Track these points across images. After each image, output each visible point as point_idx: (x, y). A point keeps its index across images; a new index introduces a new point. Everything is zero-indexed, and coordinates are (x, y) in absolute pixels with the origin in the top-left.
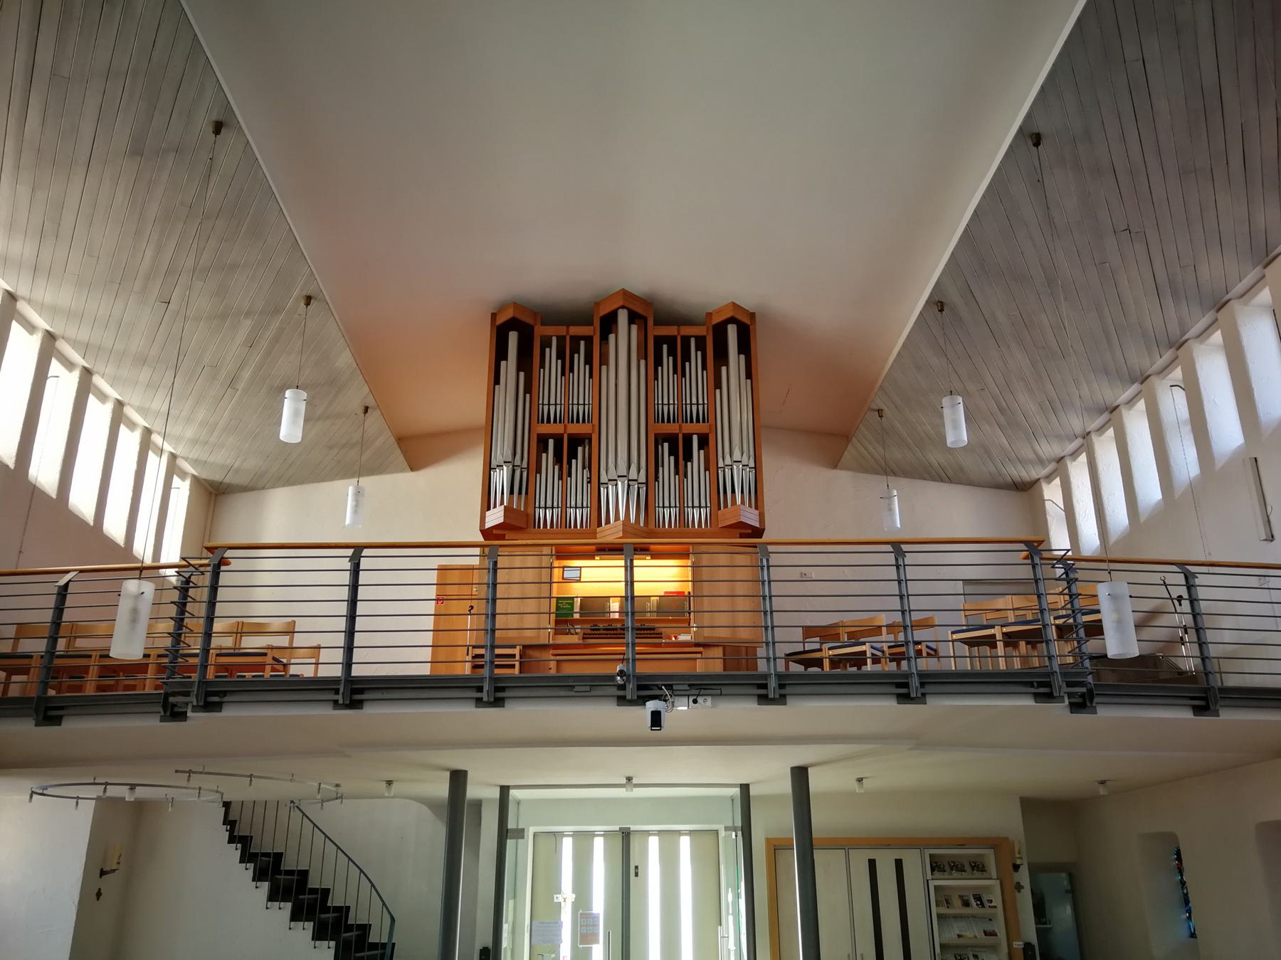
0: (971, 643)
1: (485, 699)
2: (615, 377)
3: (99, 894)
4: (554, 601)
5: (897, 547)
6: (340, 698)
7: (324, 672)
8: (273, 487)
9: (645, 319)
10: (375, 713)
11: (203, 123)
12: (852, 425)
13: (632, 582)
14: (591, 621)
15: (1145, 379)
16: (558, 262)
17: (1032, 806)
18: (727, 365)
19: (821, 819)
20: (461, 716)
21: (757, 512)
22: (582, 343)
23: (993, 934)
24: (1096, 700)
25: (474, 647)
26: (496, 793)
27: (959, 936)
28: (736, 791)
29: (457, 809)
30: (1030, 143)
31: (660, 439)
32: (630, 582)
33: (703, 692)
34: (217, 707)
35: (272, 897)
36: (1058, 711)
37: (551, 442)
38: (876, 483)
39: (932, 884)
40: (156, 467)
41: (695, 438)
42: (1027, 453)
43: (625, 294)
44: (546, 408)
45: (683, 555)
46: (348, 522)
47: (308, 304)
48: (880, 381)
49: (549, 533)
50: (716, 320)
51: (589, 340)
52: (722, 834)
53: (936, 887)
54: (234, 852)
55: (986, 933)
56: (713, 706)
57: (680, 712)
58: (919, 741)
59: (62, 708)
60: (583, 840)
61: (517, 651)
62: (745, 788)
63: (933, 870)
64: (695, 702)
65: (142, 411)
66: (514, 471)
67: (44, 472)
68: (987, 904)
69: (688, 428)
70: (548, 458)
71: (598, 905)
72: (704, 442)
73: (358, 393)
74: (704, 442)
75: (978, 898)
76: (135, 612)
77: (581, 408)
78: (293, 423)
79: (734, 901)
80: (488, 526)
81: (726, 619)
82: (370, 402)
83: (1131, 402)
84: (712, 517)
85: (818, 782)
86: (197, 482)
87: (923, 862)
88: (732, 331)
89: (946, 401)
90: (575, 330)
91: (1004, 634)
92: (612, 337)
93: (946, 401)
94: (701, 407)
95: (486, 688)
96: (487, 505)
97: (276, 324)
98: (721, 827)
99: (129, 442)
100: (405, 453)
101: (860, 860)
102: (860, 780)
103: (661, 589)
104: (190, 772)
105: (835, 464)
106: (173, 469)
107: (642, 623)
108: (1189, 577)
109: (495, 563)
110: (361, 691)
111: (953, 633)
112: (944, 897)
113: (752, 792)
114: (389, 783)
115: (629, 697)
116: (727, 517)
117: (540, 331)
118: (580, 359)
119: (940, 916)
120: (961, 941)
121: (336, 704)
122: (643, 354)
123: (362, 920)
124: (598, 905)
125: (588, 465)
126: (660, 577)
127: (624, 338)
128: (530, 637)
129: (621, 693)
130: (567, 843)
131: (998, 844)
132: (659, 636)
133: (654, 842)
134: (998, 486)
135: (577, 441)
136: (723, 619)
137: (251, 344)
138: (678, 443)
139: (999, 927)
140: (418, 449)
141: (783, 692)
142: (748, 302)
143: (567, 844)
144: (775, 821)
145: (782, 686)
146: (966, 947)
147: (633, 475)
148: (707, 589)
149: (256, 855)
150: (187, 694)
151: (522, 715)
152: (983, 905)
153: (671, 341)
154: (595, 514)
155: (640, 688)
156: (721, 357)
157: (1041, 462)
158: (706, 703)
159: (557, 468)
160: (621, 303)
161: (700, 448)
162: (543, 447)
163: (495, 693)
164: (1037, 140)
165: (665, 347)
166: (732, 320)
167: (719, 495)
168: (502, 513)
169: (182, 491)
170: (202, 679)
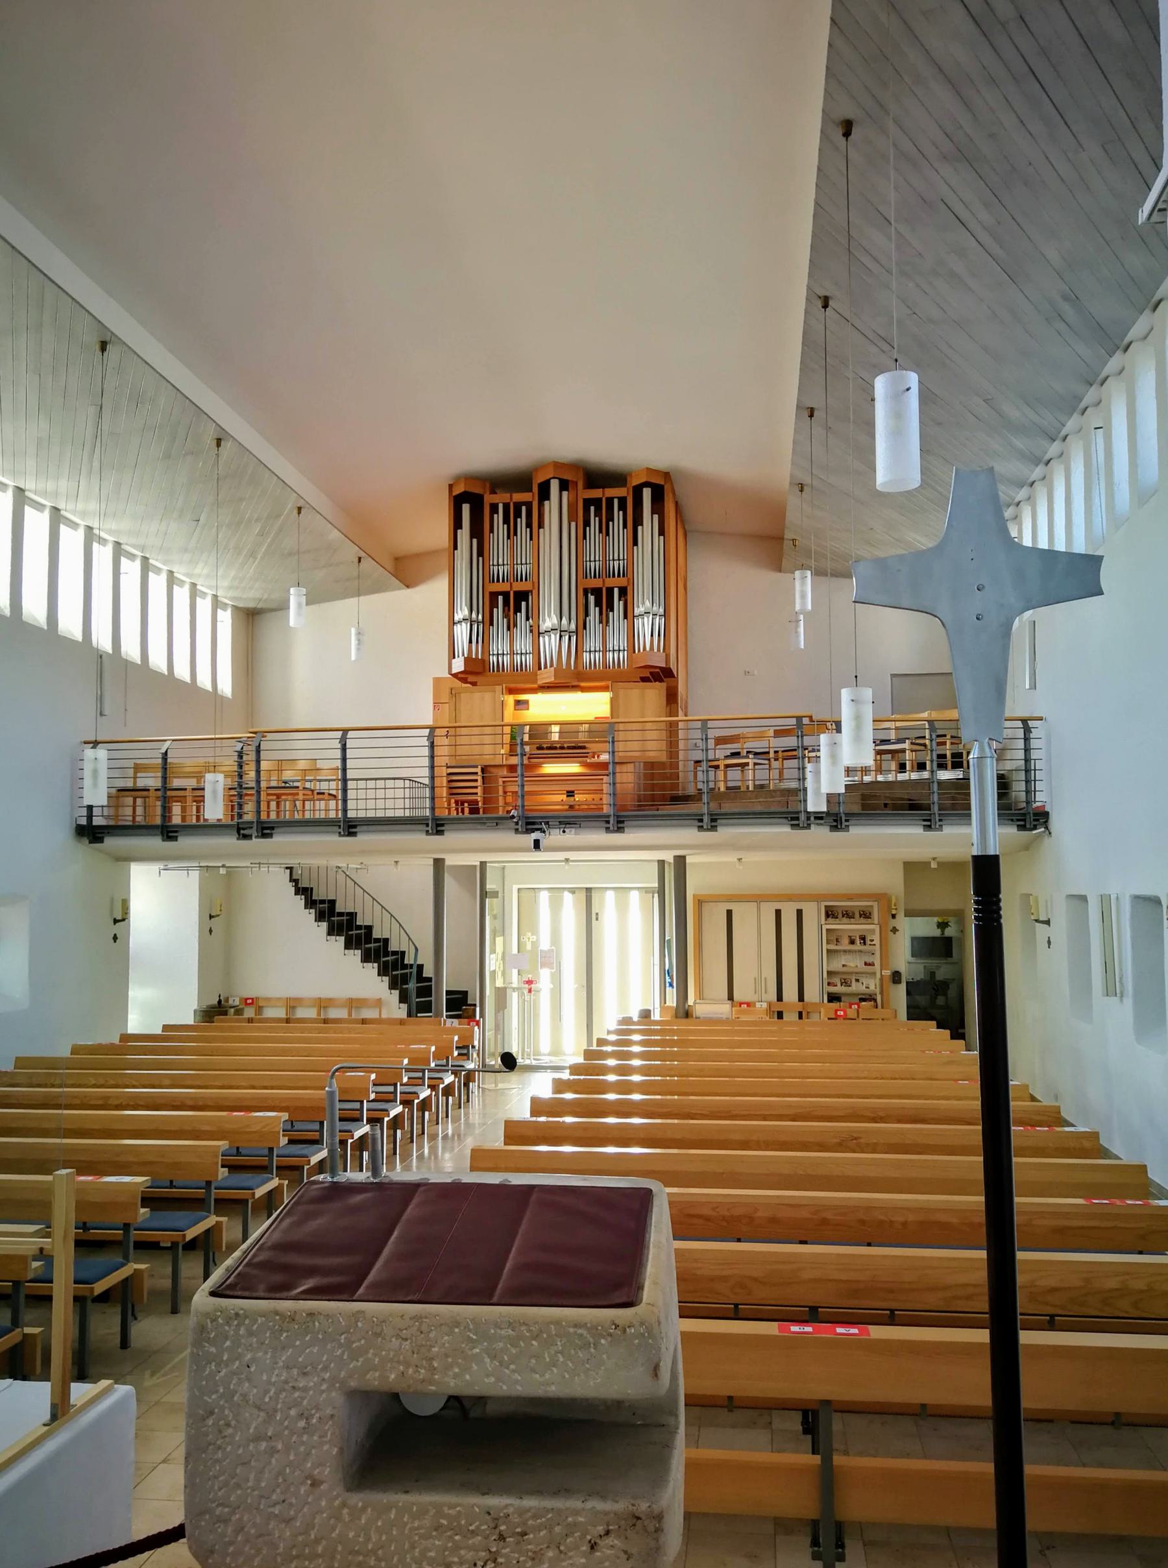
3: (211, 931)
7: (332, 815)
10: (364, 839)
14: (539, 744)
16: (494, 447)
22: (524, 508)
34: (270, 836)
35: (330, 932)
37: (500, 598)
39: (825, 927)
40: (204, 606)
43: (557, 465)
45: (605, 689)
46: (353, 658)
47: (299, 513)
50: (635, 482)
54: (300, 901)
55: (866, 964)
57: (554, 837)
61: (479, 770)
63: (827, 916)
68: (868, 942)
69: (610, 582)
70: (499, 612)
72: (623, 592)
75: (863, 938)
80: (454, 671)
87: (819, 910)
88: (647, 493)
90: (518, 497)
92: (547, 503)
106: (216, 604)
110: (355, 827)
112: (833, 937)
113: (688, 861)
114: (396, 862)
117: (489, 499)
118: (522, 522)
119: (828, 951)
120: (845, 969)
122: (572, 517)
126: (589, 706)
130: (544, 897)
131: (882, 898)
135: (522, 596)
137: (261, 534)
139: (877, 960)
140: (406, 570)
143: (544, 897)
146: (852, 973)
153: (597, 502)
155: (528, 824)
156: (638, 521)
162: (493, 604)
165: (592, 508)
166: (646, 484)
168: (462, 663)
169: (226, 618)
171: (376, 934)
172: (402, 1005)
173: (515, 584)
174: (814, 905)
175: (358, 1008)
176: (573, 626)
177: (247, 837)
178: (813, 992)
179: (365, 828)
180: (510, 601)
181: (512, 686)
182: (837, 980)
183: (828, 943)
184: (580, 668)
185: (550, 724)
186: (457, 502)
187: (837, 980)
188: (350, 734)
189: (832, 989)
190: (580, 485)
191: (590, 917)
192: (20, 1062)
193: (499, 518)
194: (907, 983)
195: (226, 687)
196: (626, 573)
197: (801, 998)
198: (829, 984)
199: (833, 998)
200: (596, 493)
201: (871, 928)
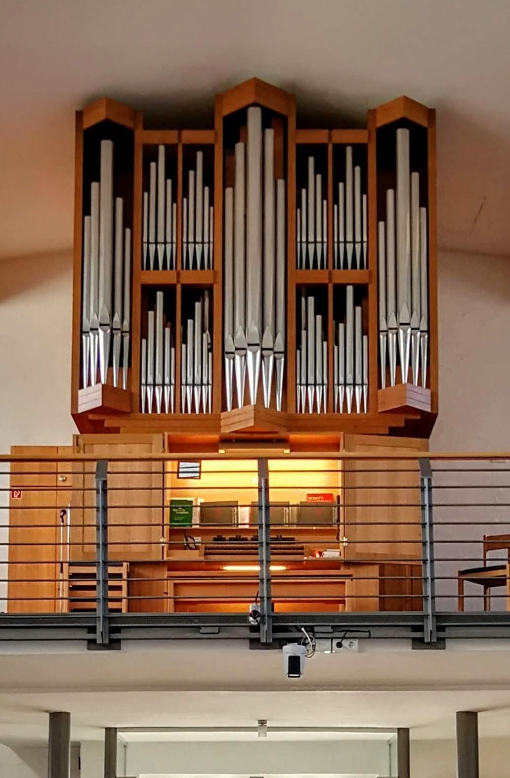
4: (167, 510)
13: (267, 489)
14: (212, 531)
18: (394, 187)
20: (71, 657)
22: (200, 155)
25: (71, 564)
26: (101, 735)
31: (304, 290)
32: (264, 488)
33: (348, 634)
37: (160, 295)
41: (350, 290)
43: (259, 85)
44: (152, 248)
49: (159, 419)
50: (382, 121)
51: (208, 150)
57: (322, 657)
61: (123, 570)
62: (404, 733)
64: (339, 645)
66: (112, 336)
69: (340, 276)
77: (199, 247)
80: (81, 409)
81: (379, 534)
88: (403, 137)
92: (239, 147)
94: (358, 247)
95: (100, 628)
96: (78, 383)
103: (299, 497)
107: (277, 532)
109: (105, 483)
117: (143, 137)
118: (196, 177)
122: (281, 171)
125: (209, 326)
126: (301, 478)
127: (257, 146)
128: (138, 552)
129: (255, 635)
132: (300, 551)
135: (194, 293)
136: (381, 533)
138: (327, 298)
145: (440, 629)
147: (268, 342)
148: (360, 496)
151: (138, 657)
153: (319, 151)
155: (276, 629)
156: (388, 179)
158: (352, 647)
159: (168, 330)
160: (251, 100)
161: (356, 303)
162: (149, 304)
163: (111, 634)
165: (311, 160)
166: (403, 123)
173: (184, 273)
176: (280, 347)
180: (178, 301)
181: (179, 434)
184: (291, 410)
185: (122, 562)
190: (292, 123)
193: (160, 167)
196: (366, 262)
200: (318, 136)
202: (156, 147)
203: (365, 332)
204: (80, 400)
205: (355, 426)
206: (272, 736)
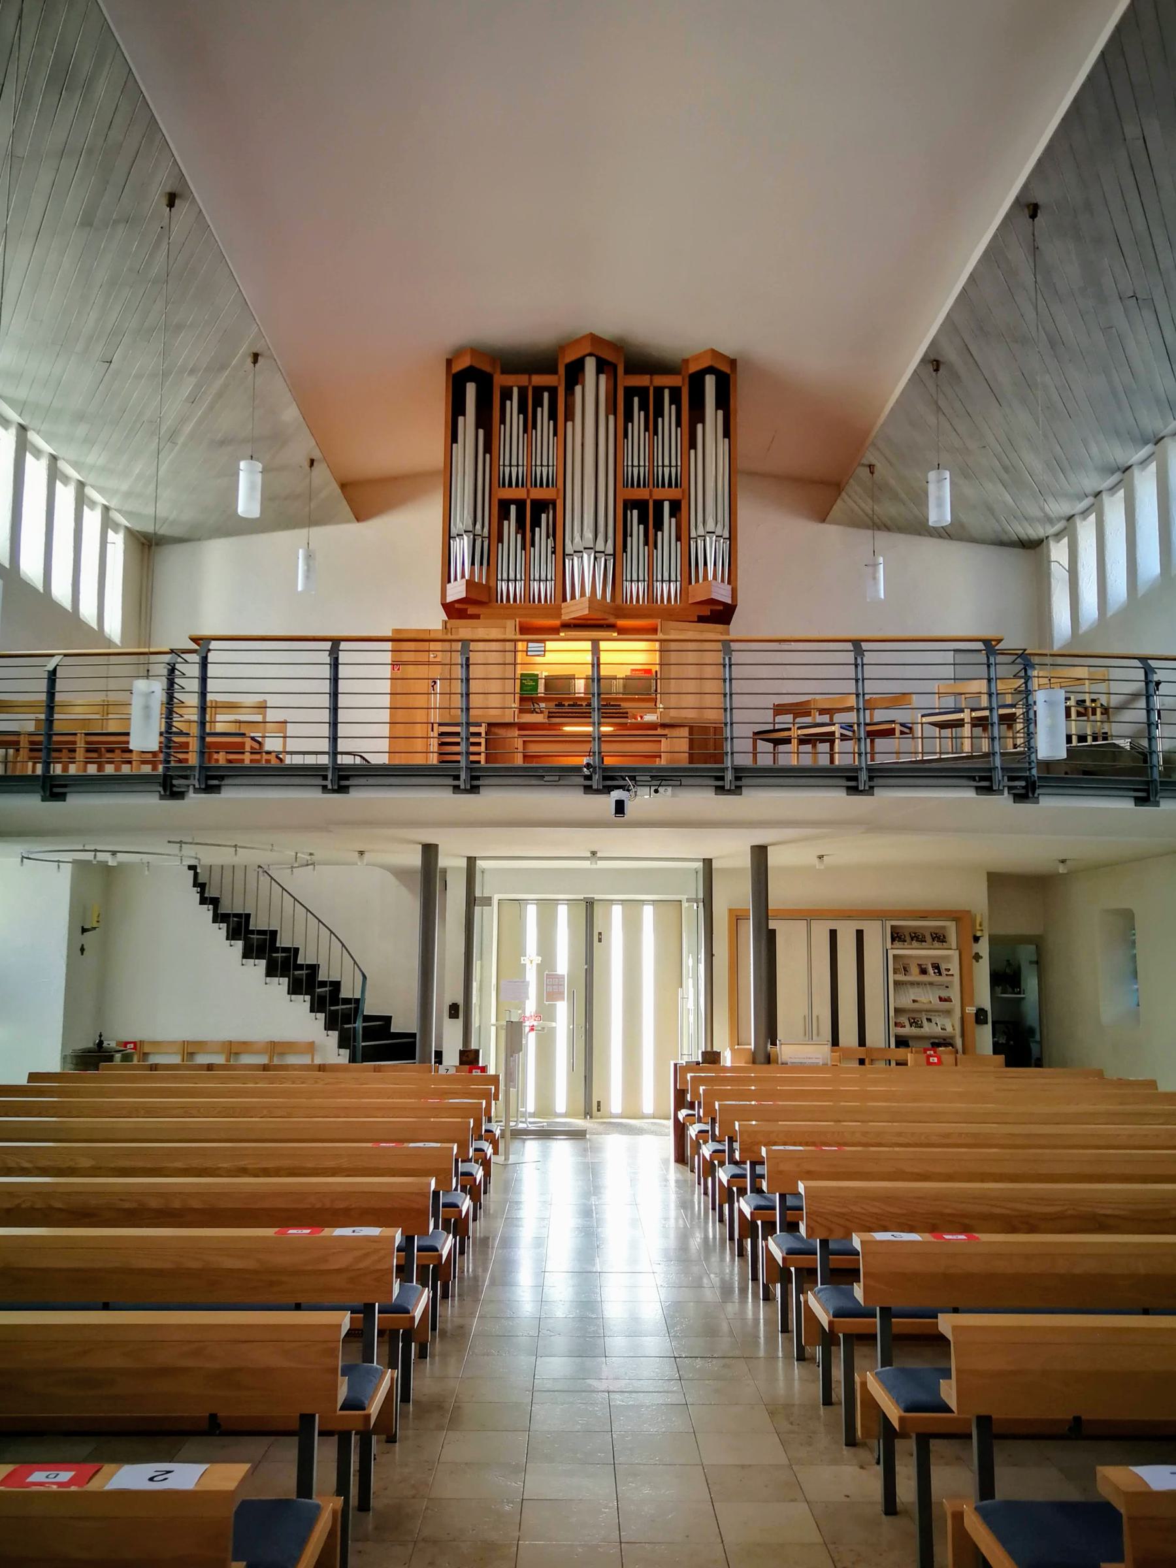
0: (942, 725)
1: (462, 787)
2: (578, 423)
3: (82, 950)
4: (518, 682)
5: (857, 643)
6: (328, 783)
8: (210, 538)
9: (614, 367)
10: (361, 797)
11: (156, 197)
12: (840, 478)
13: (599, 665)
14: (555, 700)
15: (1158, 441)
16: (518, 310)
17: (998, 881)
19: (778, 895)
20: (439, 800)
21: (730, 587)
22: (546, 395)
23: (948, 1000)
24: (1038, 791)
25: (440, 725)
26: (463, 863)
27: (914, 1001)
28: (699, 865)
29: (429, 877)
30: (1026, 212)
31: (629, 505)
32: (596, 664)
34: (215, 789)
35: (246, 955)
36: (1003, 801)
37: (513, 508)
38: (864, 536)
40: (92, 520)
41: (666, 505)
42: (1032, 510)
43: (594, 339)
44: (507, 470)
46: (300, 589)
47: (255, 361)
48: (874, 433)
49: (511, 607)
50: (693, 368)
51: (553, 391)
52: (685, 905)
53: (894, 956)
54: (207, 912)
55: (941, 999)
56: (673, 796)
57: (642, 801)
58: (872, 826)
59: (65, 786)
60: (547, 908)
61: (482, 730)
62: (708, 863)
63: (893, 940)
64: (656, 791)
65: (76, 465)
66: (474, 540)
67: (31, 567)
68: (944, 972)
69: (659, 493)
71: (562, 966)
72: (676, 508)
73: (303, 446)
74: (676, 508)
75: (936, 967)
76: (147, 707)
77: (545, 470)
78: (250, 497)
79: (693, 965)
80: (449, 599)
81: (689, 700)
82: (317, 454)
83: (1144, 463)
84: (684, 592)
85: (774, 858)
86: (131, 534)
88: (710, 382)
89: (932, 475)
90: (539, 380)
91: (972, 718)
92: (578, 389)
93: (932, 475)
95: (463, 776)
96: (447, 578)
97: (221, 381)
98: (684, 897)
99: (65, 495)
100: (350, 501)
101: (821, 932)
102: (821, 857)
104: (181, 842)
105: (823, 520)
106: (107, 523)
107: (606, 701)
108: (1148, 671)
109: (468, 659)
110: (347, 778)
111: (923, 716)
112: (902, 966)
113: (714, 866)
114: (361, 853)
115: (595, 787)
116: (698, 593)
117: (500, 380)
119: (896, 983)
120: (916, 1006)
121: (325, 789)
122: (612, 409)
123: (334, 977)
124: (562, 966)
125: (552, 534)
127: (592, 388)
128: (495, 716)
129: (588, 783)
130: (532, 911)
131: (959, 917)
133: (617, 911)
134: (1001, 543)
135: (540, 506)
136: (690, 701)
137: (193, 400)
138: (648, 511)
140: (363, 497)
141: (739, 783)
142: (728, 347)
143: (532, 911)
144: (734, 893)
145: (738, 778)
146: (919, 1011)
148: (674, 671)
149: (228, 915)
150: (186, 777)
151: (494, 800)
152: (940, 974)
153: (642, 392)
154: (560, 587)
155: (605, 778)
156: (698, 415)
157: (1050, 520)
158: (666, 793)
159: (519, 536)
160: (588, 351)
161: (672, 515)
162: (504, 515)
164: (1034, 211)
165: (636, 400)
166: (710, 370)
167: (689, 569)
168: (464, 587)
169: (117, 542)
170: (205, 763)
171: (322, 976)
172: (342, 1051)
174: (877, 924)
175: (282, 1054)
176: (610, 550)
177: (177, 795)
178: (877, 1035)
179: (362, 781)
180: (526, 513)
182: (904, 1020)
183: (895, 973)
184: (619, 601)
186: (457, 383)
187: (904, 1020)
188: (343, 645)
189: (901, 1031)
191: (590, 938)
192: (33, 1077)
193: (513, 405)
194: (994, 1023)
195: (113, 627)
197: (862, 1042)
198: (896, 1024)
199: (902, 1042)
201: (949, 956)
202: (511, 389)
203: (678, 539)
204: (449, 592)
205: (670, 614)
206: (602, 864)
